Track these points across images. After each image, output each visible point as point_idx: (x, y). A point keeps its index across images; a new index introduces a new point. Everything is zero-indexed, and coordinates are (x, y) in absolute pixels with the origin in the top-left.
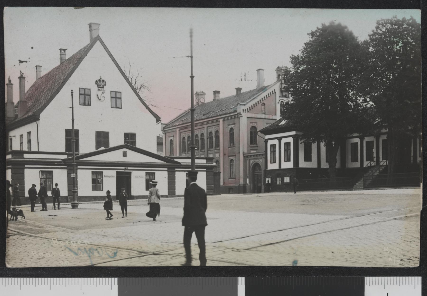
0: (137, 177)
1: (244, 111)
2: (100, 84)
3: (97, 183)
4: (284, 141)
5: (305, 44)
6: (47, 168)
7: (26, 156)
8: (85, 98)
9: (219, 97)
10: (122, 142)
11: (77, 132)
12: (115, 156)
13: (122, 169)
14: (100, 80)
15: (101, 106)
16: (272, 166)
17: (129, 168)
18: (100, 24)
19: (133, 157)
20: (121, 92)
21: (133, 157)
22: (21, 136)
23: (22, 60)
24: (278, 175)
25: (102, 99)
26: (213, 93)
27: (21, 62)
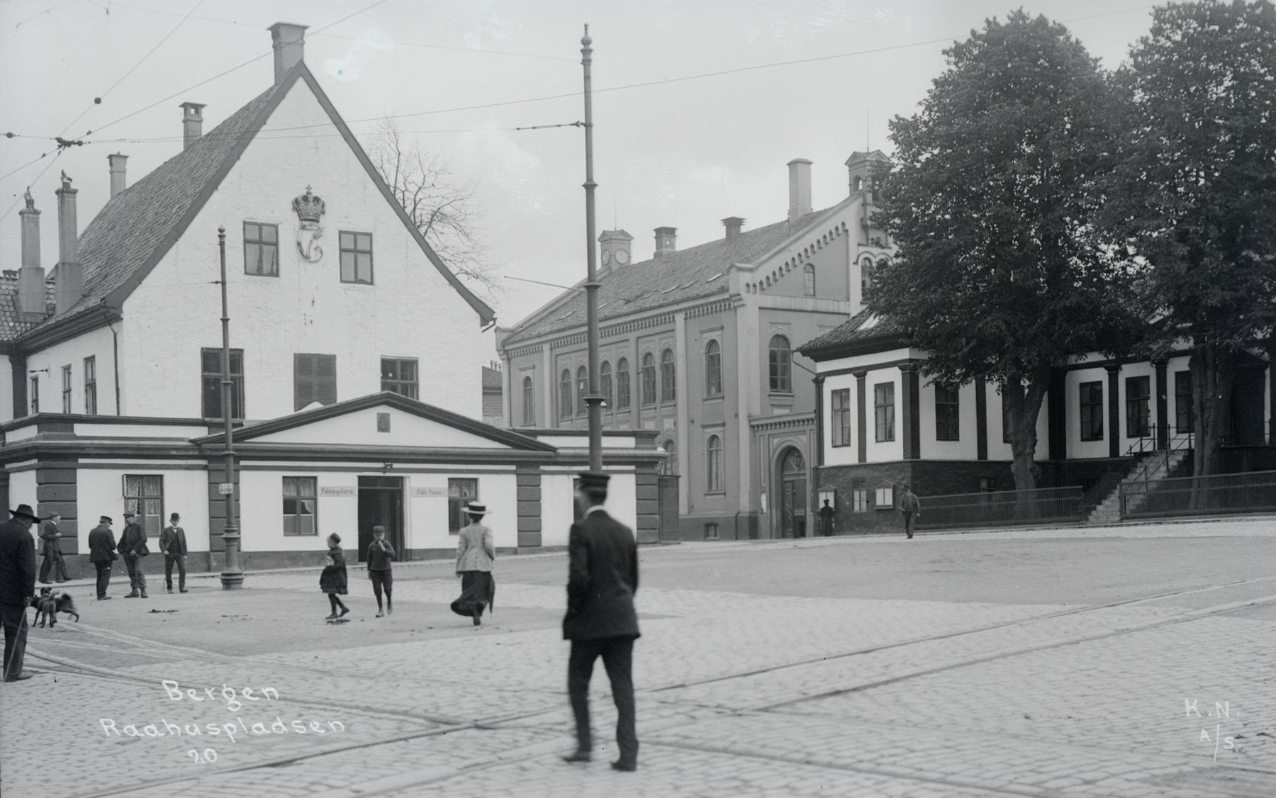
0: (422, 492)
1: (752, 288)
2: (308, 209)
3: (298, 511)
4: (873, 378)
5: (936, 82)
6: (146, 467)
7: (80, 430)
8: (262, 252)
9: (672, 245)
10: (372, 385)
11: (239, 353)
12: (356, 431)
13: (374, 469)
14: (305, 198)
15: (310, 279)
16: (835, 457)
17: (395, 466)
18: (305, 28)
19: (409, 432)
20: (370, 235)
21: (409, 432)
22: (67, 369)
23: (67, 138)
24: (857, 483)
25: (314, 255)
26: (654, 234)
27: (63, 143)
